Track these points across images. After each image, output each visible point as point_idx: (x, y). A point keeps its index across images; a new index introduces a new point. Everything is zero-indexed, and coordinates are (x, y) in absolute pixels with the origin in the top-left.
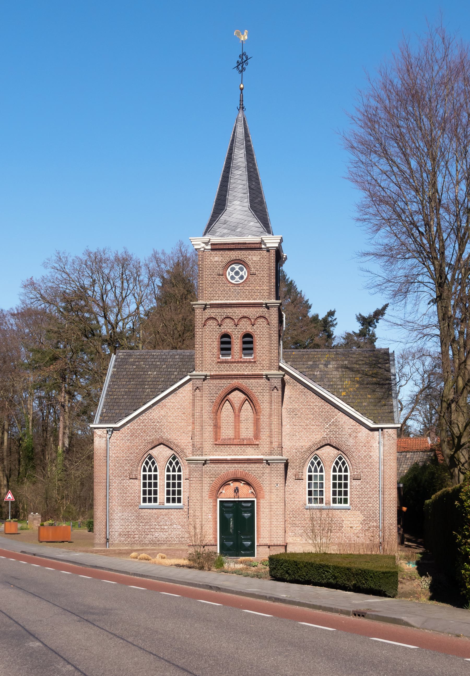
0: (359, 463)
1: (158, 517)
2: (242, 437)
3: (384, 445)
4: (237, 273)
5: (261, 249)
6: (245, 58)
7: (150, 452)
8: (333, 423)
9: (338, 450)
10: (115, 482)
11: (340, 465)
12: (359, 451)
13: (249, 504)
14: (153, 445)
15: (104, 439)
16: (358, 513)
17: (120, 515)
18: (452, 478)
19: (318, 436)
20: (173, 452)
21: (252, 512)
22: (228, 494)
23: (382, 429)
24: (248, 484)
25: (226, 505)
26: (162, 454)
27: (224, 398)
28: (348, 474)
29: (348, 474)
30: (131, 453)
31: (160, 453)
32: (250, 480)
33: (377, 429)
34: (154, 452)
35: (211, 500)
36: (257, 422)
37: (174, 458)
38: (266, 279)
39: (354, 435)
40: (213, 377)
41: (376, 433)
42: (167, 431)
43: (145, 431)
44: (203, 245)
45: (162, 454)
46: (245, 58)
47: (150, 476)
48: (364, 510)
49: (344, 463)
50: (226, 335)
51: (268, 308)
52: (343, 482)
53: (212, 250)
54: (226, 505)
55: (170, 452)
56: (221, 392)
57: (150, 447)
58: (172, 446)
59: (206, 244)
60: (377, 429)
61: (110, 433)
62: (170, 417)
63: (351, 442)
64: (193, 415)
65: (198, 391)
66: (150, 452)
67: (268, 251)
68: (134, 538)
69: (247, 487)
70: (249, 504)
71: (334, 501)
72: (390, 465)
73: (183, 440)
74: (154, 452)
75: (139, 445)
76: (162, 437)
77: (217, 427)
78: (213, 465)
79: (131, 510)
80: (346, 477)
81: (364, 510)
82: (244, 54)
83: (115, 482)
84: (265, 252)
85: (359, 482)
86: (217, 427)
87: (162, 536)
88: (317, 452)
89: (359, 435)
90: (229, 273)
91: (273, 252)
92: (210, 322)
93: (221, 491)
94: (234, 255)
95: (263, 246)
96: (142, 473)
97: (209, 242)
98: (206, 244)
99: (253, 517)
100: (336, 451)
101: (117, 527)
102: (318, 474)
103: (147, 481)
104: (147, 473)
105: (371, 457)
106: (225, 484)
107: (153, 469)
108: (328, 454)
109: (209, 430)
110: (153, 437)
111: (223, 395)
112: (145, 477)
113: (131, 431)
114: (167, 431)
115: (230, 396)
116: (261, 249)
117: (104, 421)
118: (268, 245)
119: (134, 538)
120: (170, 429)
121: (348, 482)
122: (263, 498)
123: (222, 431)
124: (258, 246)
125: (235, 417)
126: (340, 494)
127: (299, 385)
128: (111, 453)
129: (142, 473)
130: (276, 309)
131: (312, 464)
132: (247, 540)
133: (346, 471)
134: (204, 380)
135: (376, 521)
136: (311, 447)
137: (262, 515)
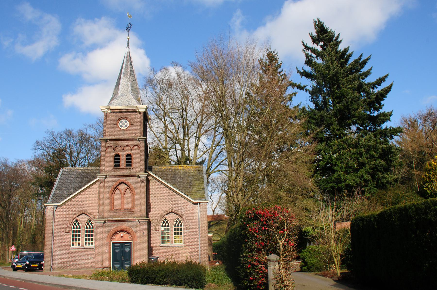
0: (188, 221)
1: (80, 253)
2: (125, 208)
3: (201, 212)
4: (124, 124)
5: (136, 112)
6: (130, 25)
7: (77, 218)
8: (174, 201)
9: (177, 214)
10: (57, 235)
11: (178, 223)
12: (188, 215)
13: (129, 244)
14: (79, 214)
15: (52, 211)
16: (188, 247)
17: (59, 252)
18: (13, 267)
19: (166, 208)
20: (89, 218)
21: (130, 248)
22: (118, 239)
23: (200, 203)
24: (128, 233)
25: (116, 245)
26: (83, 219)
27: (116, 188)
28: (183, 227)
29: (183, 227)
30: (67, 219)
31: (83, 218)
32: (129, 231)
33: (197, 204)
34: (79, 218)
35: (108, 243)
36: (133, 200)
37: (90, 221)
38: (138, 124)
39: (185, 207)
40: (110, 176)
41: (197, 205)
42: (87, 206)
43: (74, 207)
44: (106, 110)
45: (83, 219)
46: (130, 25)
47: (90, 231)
48: (191, 246)
49: (180, 222)
50: (118, 155)
51: (139, 141)
52: (180, 231)
53: (111, 112)
54: (116, 245)
55: (88, 218)
56: (115, 185)
57: (77, 215)
58: (89, 214)
59: (108, 109)
60: (197, 204)
61: (55, 208)
62: (88, 199)
63: (184, 210)
64: (99, 197)
65: (102, 184)
66: (77, 218)
67: (140, 113)
68: (66, 265)
69: (127, 234)
70: (129, 244)
71: (162, 243)
72: (204, 222)
73: (94, 211)
74: (79, 218)
75: (71, 214)
76: (83, 210)
77: (112, 203)
78: (109, 223)
79: (65, 250)
80: (181, 229)
81: (191, 246)
82: (130, 23)
83: (57, 235)
84: (138, 114)
85: (188, 231)
86: (112, 203)
87: (83, 263)
88: (166, 216)
89: (188, 207)
90: (120, 124)
91: (142, 115)
92: (109, 148)
93: (113, 237)
94: (121, 115)
95: (137, 111)
96: (72, 229)
97: (110, 108)
98: (108, 109)
99: (130, 251)
100: (176, 215)
101: (57, 259)
102: (167, 227)
103: (88, 233)
104: (88, 229)
105: (194, 218)
106: (115, 233)
107: (78, 227)
108: (172, 217)
109: (107, 204)
110: (79, 209)
111: (115, 186)
112: (74, 231)
113: (67, 207)
114: (87, 206)
115: (119, 187)
116: (136, 112)
117: (210, 242)
118: (140, 110)
119: (66, 265)
120: (88, 205)
121: (183, 231)
122: (136, 240)
123: (115, 204)
124: (134, 111)
125: (122, 197)
126: (89, 240)
127: (157, 182)
128: (56, 219)
129: (72, 229)
130: (144, 142)
131: (164, 222)
132: (127, 264)
133: (181, 225)
134: (105, 178)
135: (197, 252)
136: (163, 214)
137: (135, 250)
